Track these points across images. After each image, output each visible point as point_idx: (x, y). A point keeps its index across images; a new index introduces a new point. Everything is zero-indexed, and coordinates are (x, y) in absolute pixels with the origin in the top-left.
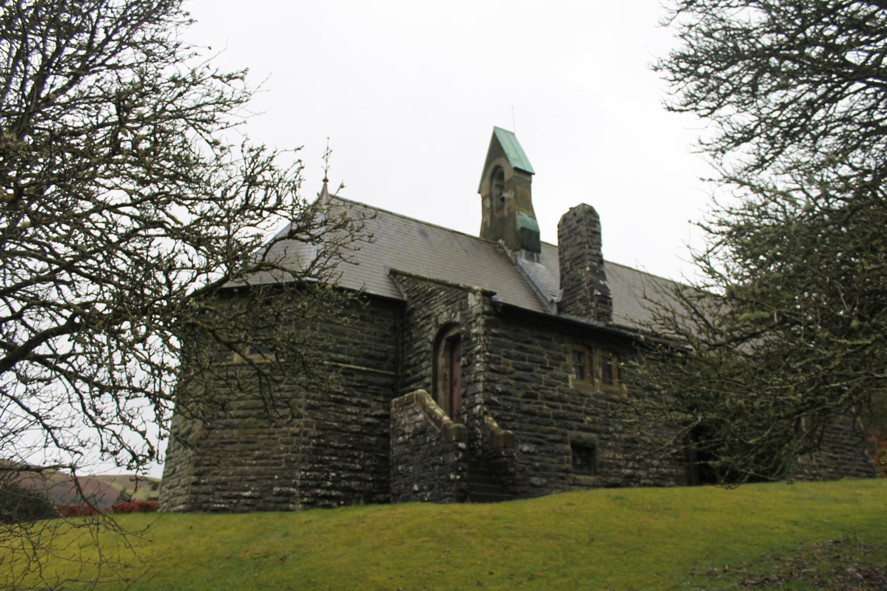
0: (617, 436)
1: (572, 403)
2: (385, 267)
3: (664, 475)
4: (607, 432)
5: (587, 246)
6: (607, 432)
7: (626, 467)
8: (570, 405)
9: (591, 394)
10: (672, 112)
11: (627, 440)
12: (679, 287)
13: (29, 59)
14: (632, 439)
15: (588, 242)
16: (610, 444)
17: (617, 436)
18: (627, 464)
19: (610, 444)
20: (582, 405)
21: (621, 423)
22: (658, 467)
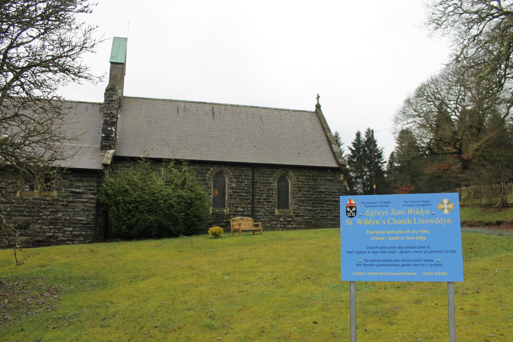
0: (45, 217)
1: (17, 204)
2: (395, 138)
3: (76, 235)
4: (38, 216)
5: (105, 109)
6: (38, 216)
7: (49, 232)
8: (16, 205)
9: (31, 198)
10: (366, 267)
11: (51, 219)
12: (106, 96)
13: (397, 145)
14: (55, 218)
15: (105, 107)
16: (39, 222)
17: (45, 217)
18: (50, 231)
19: (39, 222)
20: (23, 204)
21: (49, 211)
22: (71, 231)
